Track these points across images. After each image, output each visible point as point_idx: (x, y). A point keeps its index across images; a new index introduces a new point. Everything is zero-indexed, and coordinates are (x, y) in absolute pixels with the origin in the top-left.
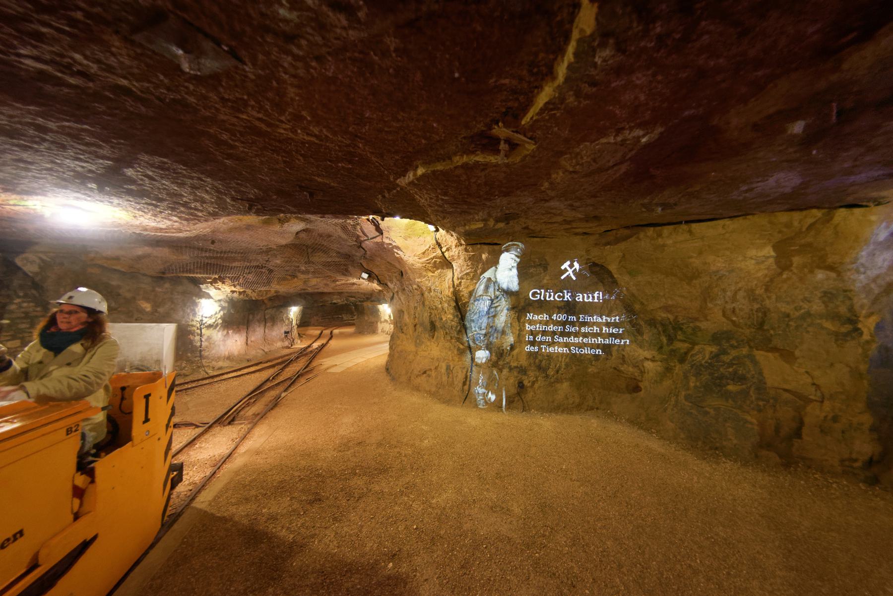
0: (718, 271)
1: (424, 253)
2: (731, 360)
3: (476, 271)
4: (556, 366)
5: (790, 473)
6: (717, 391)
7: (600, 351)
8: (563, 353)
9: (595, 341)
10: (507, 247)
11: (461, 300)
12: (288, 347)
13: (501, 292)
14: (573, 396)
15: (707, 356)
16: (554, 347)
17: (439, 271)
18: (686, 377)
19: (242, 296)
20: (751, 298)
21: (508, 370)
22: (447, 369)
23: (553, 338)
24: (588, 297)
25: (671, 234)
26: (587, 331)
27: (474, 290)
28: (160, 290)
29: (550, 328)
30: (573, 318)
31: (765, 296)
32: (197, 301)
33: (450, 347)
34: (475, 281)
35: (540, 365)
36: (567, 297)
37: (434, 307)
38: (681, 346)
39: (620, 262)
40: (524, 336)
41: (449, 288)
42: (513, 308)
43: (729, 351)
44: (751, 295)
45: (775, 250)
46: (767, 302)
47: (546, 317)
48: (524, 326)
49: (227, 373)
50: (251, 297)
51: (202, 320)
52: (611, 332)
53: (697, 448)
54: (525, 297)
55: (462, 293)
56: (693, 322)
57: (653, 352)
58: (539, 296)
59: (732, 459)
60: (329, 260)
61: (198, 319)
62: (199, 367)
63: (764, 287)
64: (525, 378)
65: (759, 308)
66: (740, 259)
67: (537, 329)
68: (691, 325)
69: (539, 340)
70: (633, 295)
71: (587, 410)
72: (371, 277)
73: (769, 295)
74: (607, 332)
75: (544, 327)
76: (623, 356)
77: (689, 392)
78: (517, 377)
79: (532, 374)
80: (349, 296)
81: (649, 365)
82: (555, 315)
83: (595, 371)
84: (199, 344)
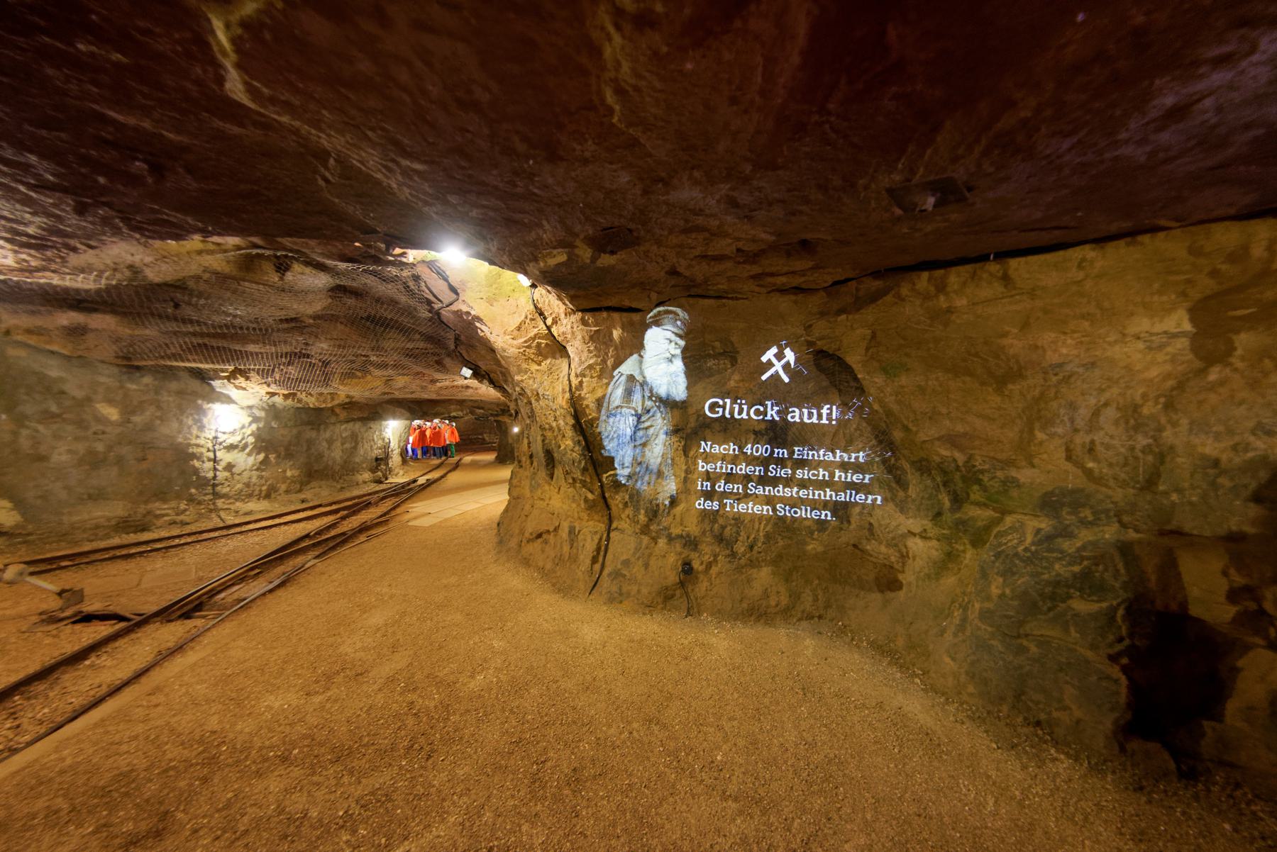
0: (1061, 365)
1: (519, 328)
2: (1079, 550)
3: (604, 362)
4: (748, 538)
5: (1196, 797)
6: (1045, 608)
7: (829, 514)
8: (762, 516)
9: (819, 495)
10: (655, 316)
11: (585, 414)
12: (379, 482)
13: (655, 402)
14: (778, 592)
15: (1029, 539)
16: (747, 504)
17: (548, 361)
18: (984, 574)
19: (289, 402)
20: (1132, 422)
21: (666, 541)
22: (570, 532)
23: (745, 488)
24: (810, 415)
25: (964, 283)
26: (806, 477)
27: (604, 396)
28: (134, 387)
29: (741, 469)
30: (782, 452)
31: (1163, 420)
32: (206, 406)
33: (574, 496)
34: (605, 381)
35: (721, 534)
36: (772, 413)
37: (547, 426)
38: (978, 514)
39: (867, 349)
40: (695, 482)
41: (564, 391)
42: (676, 431)
43: (1076, 532)
44: (1132, 416)
45: (1193, 320)
46: (1168, 434)
47: (734, 450)
48: (696, 464)
49: (256, 521)
50: (308, 404)
51: (216, 438)
52: (849, 480)
53: (999, 717)
54: (697, 411)
55: (585, 403)
56: (1002, 469)
57: (925, 522)
58: (721, 410)
59: (1072, 752)
60: (410, 345)
61: (209, 434)
62: (211, 511)
63: (1162, 400)
64: (694, 555)
65: (1149, 446)
66: (1111, 339)
67: (718, 470)
68: (999, 474)
69: (722, 489)
70: (889, 413)
71: (799, 620)
72: (477, 374)
73: (1175, 417)
74: (843, 479)
75: (729, 466)
76: (871, 524)
77: (987, 605)
78: (680, 554)
79: (707, 549)
80: (475, 407)
81: (916, 544)
82: (749, 446)
83: (820, 549)
84: (211, 475)
